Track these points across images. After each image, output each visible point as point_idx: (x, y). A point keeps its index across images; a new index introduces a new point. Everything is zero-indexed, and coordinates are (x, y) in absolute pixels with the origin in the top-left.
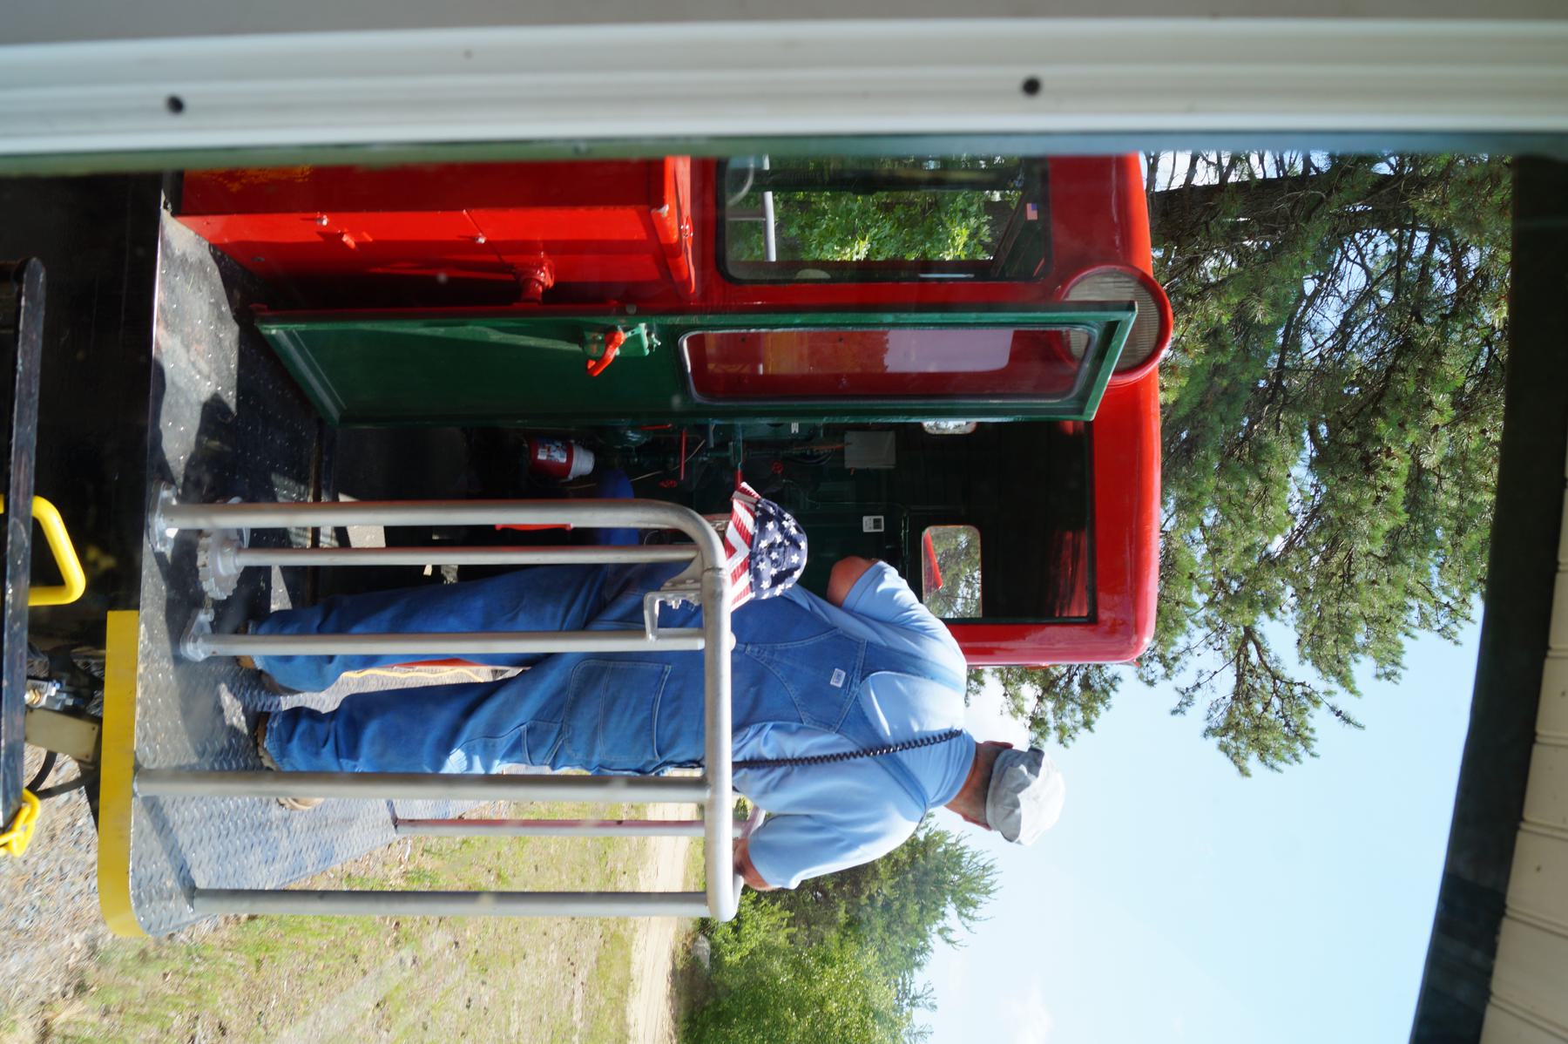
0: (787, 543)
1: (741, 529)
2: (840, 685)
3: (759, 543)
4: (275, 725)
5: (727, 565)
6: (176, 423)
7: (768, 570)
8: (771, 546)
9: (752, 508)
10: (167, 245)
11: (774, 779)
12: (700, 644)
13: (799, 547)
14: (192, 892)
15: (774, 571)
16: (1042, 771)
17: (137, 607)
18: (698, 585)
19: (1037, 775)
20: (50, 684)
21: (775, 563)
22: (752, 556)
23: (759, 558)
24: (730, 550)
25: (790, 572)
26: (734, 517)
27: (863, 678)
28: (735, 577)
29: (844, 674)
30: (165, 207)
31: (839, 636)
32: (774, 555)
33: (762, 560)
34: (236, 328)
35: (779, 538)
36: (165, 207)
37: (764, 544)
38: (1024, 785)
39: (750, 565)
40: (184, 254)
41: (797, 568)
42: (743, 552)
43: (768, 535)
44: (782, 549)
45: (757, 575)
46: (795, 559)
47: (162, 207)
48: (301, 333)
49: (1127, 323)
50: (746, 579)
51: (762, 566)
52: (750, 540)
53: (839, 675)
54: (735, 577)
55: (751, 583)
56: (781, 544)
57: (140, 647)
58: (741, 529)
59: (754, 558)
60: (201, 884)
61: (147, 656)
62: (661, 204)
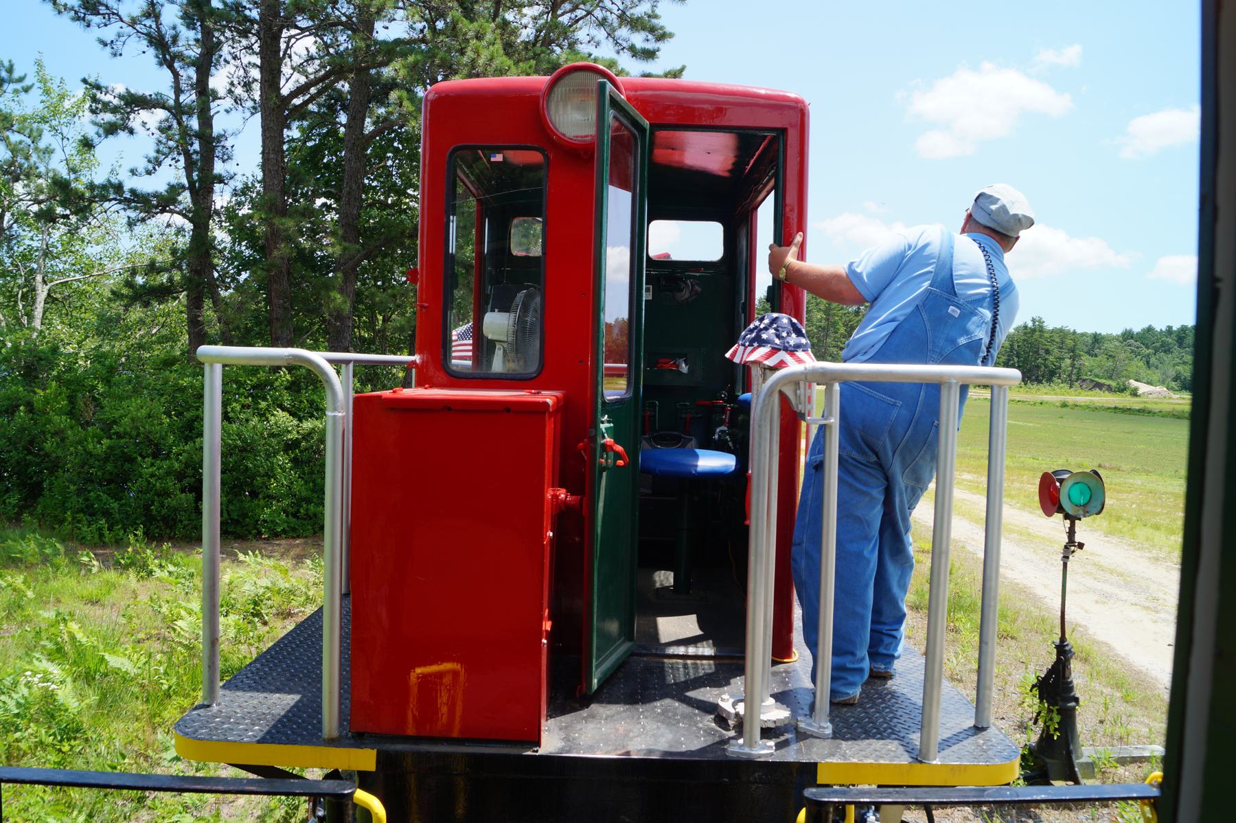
0: (775, 326)
1: (769, 356)
2: (959, 311)
3: (776, 344)
4: (883, 667)
5: (793, 367)
6: (682, 743)
7: (793, 339)
8: (778, 336)
9: (750, 349)
10: (562, 750)
11: (857, 333)
12: (218, 368)
13: (777, 318)
14: (978, 729)
15: (794, 335)
16: (996, 196)
17: (815, 765)
18: (802, 384)
19: (998, 199)
20: (868, 819)
21: (789, 334)
22: (786, 349)
23: (786, 345)
24: (782, 364)
25: (793, 325)
26: (761, 360)
27: (955, 294)
28: (800, 361)
29: (951, 307)
30: (537, 751)
31: (924, 305)
32: (784, 334)
33: (788, 343)
34: (592, 705)
35: (772, 331)
36: (537, 751)
37: (777, 341)
38: (1004, 209)
39: (792, 351)
40: (563, 740)
41: (791, 321)
42: (782, 355)
43: (771, 338)
44: (780, 329)
45: (798, 346)
46: (785, 321)
47: (537, 754)
48: (597, 661)
49: (611, 89)
50: (800, 354)
51: (792, 343)
52: (775, 350)
53: (953, 311)
54: (800, 361)
55: (803, 351)
56: (776, 329)
57: (839, 761)
58: (769, 356)
59: (787, 347)
60: (971, 723)
61: (844, 756)
62: (546, 404)
